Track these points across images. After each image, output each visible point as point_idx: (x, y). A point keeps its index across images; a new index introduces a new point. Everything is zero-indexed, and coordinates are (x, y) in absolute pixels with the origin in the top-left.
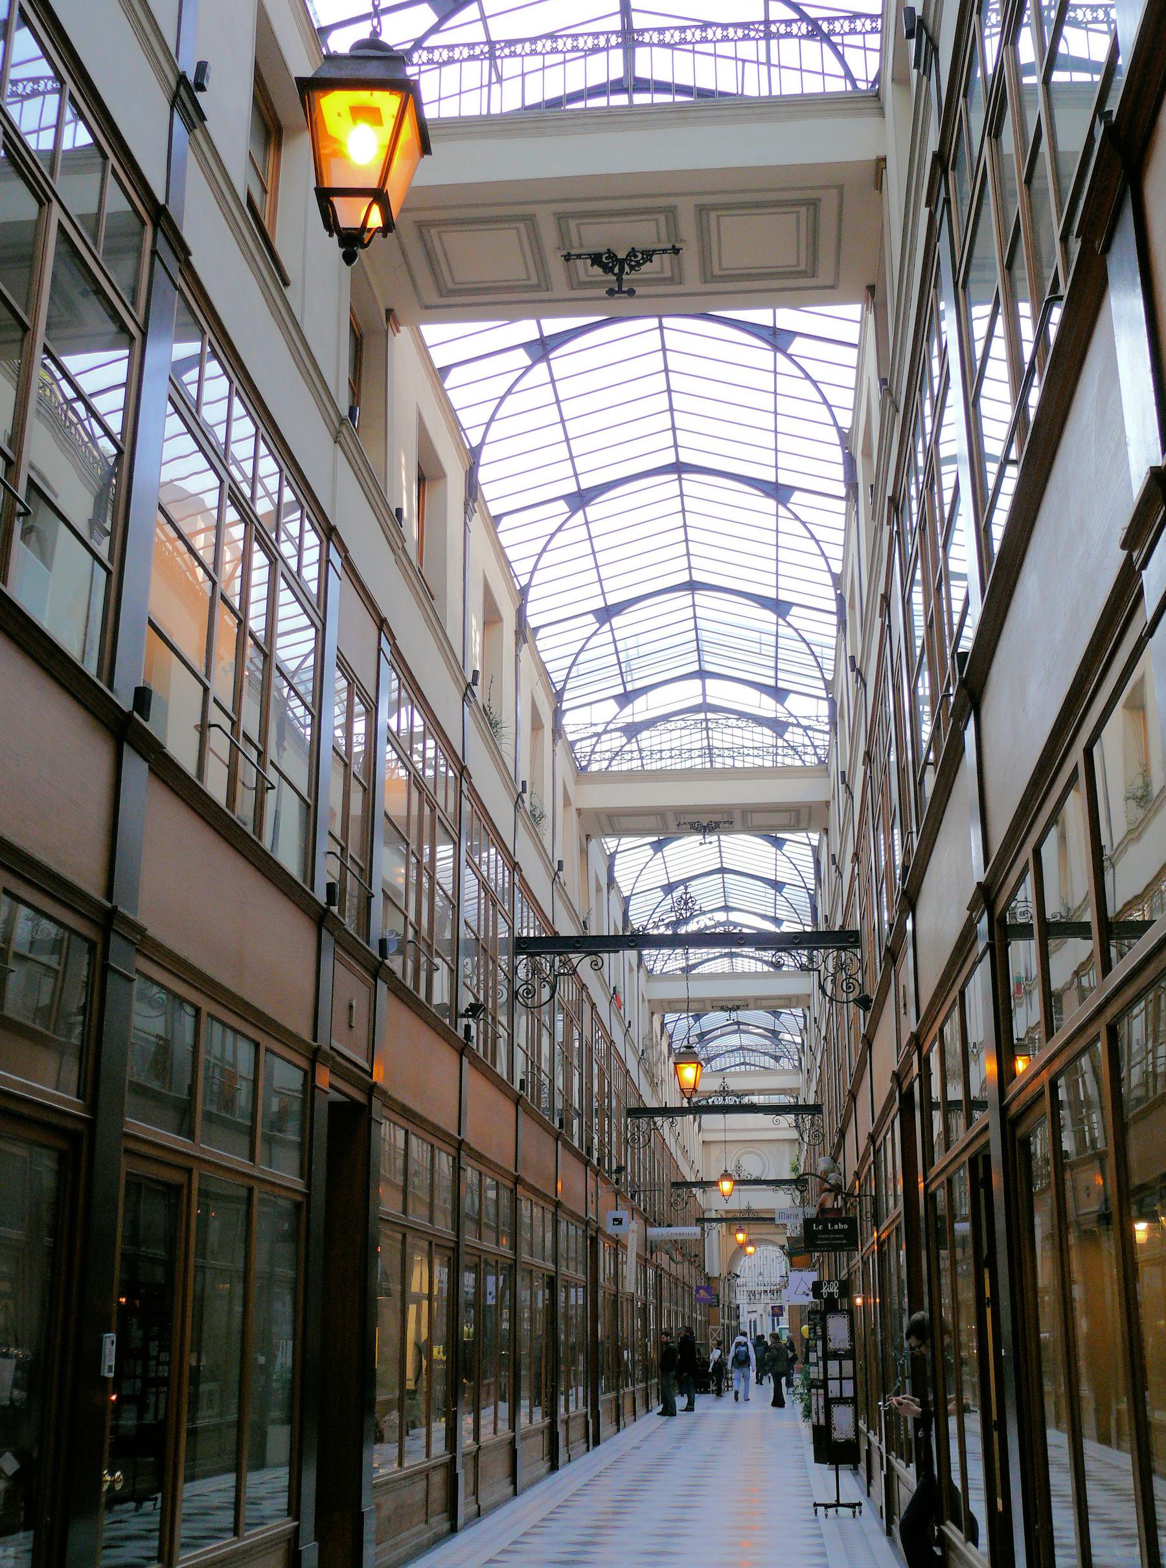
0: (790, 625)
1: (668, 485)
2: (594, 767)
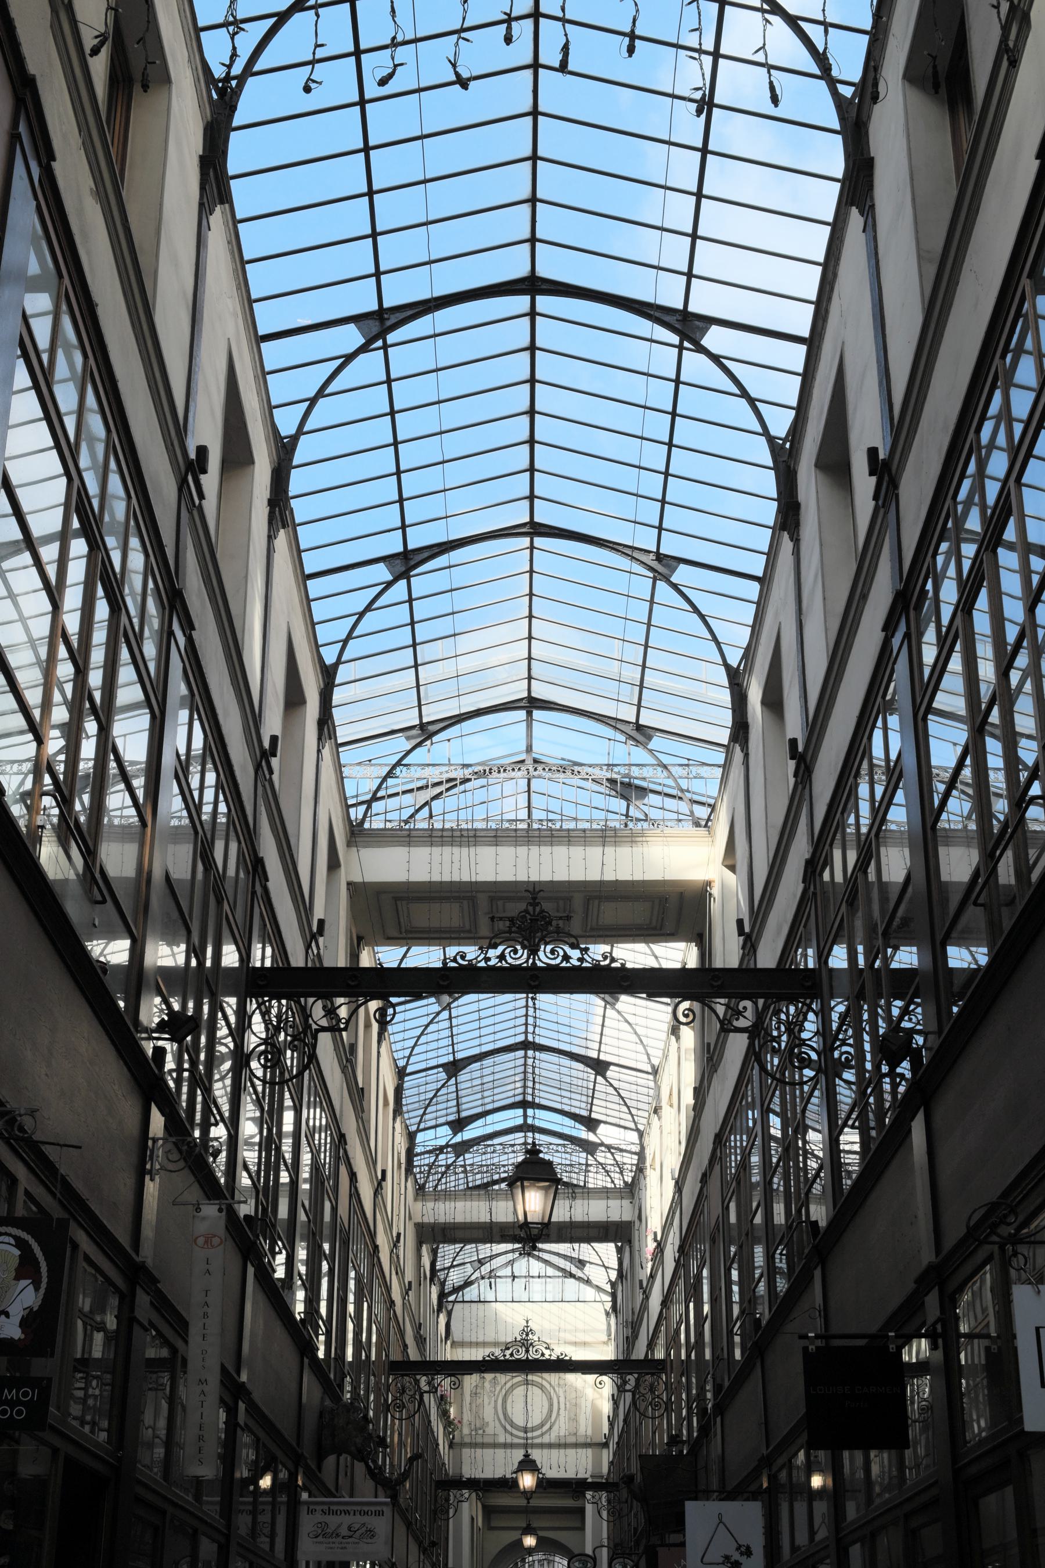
1: (503, 323)
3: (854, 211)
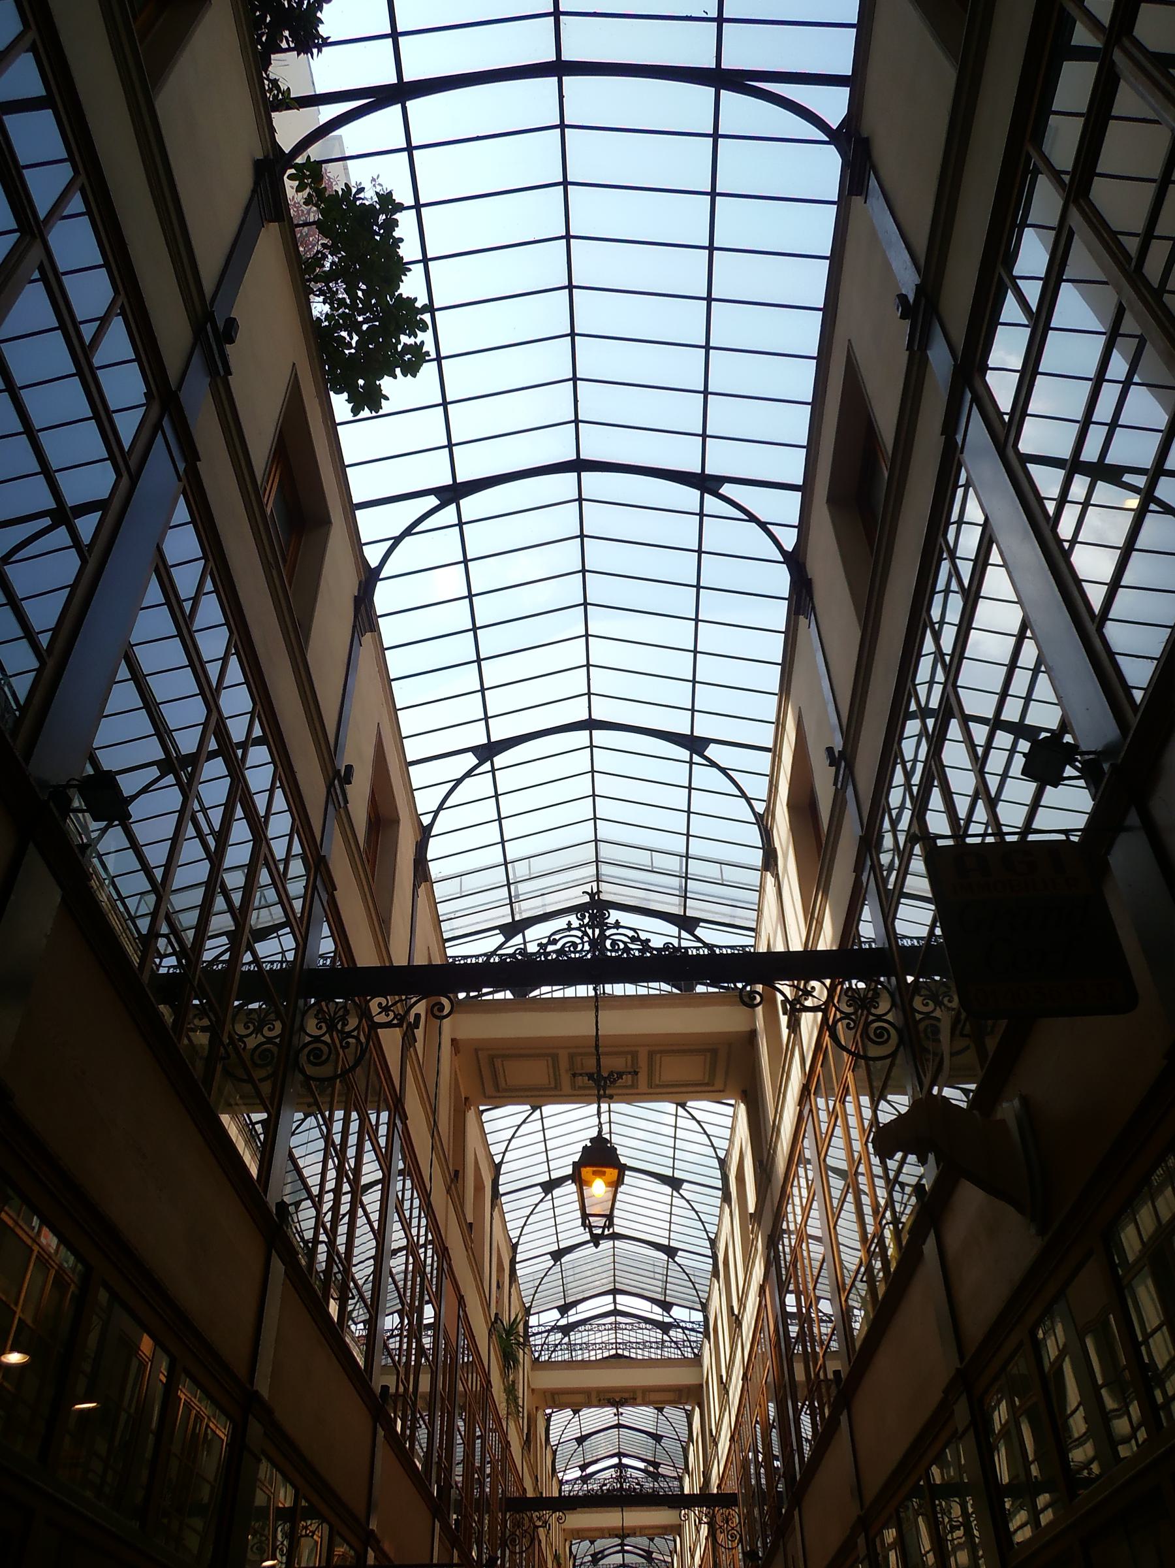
0: (683, 1197)
1: (569, 754)
2: (542, 1359)
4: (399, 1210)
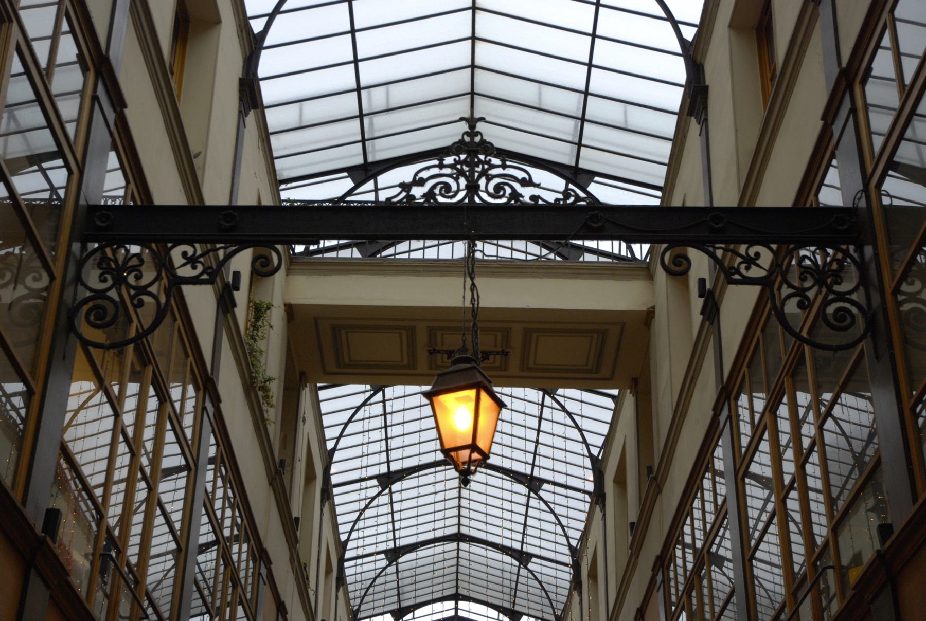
3: (693, 120)
4: (209, 501)
